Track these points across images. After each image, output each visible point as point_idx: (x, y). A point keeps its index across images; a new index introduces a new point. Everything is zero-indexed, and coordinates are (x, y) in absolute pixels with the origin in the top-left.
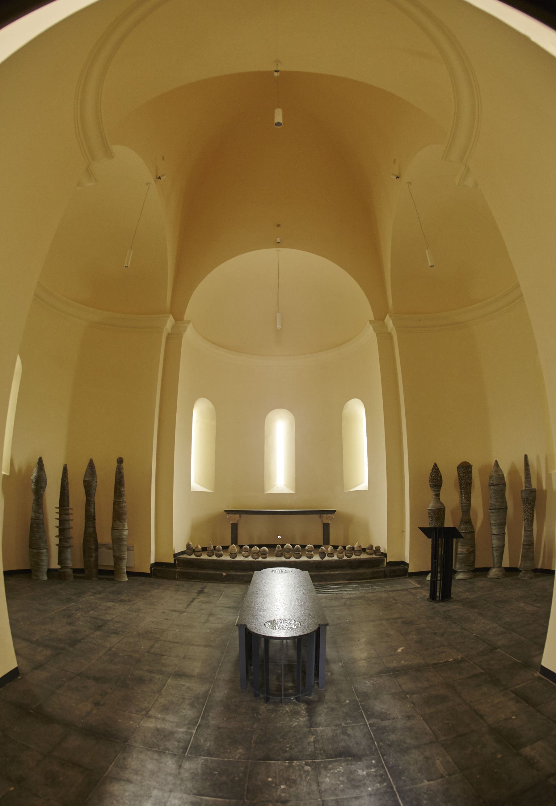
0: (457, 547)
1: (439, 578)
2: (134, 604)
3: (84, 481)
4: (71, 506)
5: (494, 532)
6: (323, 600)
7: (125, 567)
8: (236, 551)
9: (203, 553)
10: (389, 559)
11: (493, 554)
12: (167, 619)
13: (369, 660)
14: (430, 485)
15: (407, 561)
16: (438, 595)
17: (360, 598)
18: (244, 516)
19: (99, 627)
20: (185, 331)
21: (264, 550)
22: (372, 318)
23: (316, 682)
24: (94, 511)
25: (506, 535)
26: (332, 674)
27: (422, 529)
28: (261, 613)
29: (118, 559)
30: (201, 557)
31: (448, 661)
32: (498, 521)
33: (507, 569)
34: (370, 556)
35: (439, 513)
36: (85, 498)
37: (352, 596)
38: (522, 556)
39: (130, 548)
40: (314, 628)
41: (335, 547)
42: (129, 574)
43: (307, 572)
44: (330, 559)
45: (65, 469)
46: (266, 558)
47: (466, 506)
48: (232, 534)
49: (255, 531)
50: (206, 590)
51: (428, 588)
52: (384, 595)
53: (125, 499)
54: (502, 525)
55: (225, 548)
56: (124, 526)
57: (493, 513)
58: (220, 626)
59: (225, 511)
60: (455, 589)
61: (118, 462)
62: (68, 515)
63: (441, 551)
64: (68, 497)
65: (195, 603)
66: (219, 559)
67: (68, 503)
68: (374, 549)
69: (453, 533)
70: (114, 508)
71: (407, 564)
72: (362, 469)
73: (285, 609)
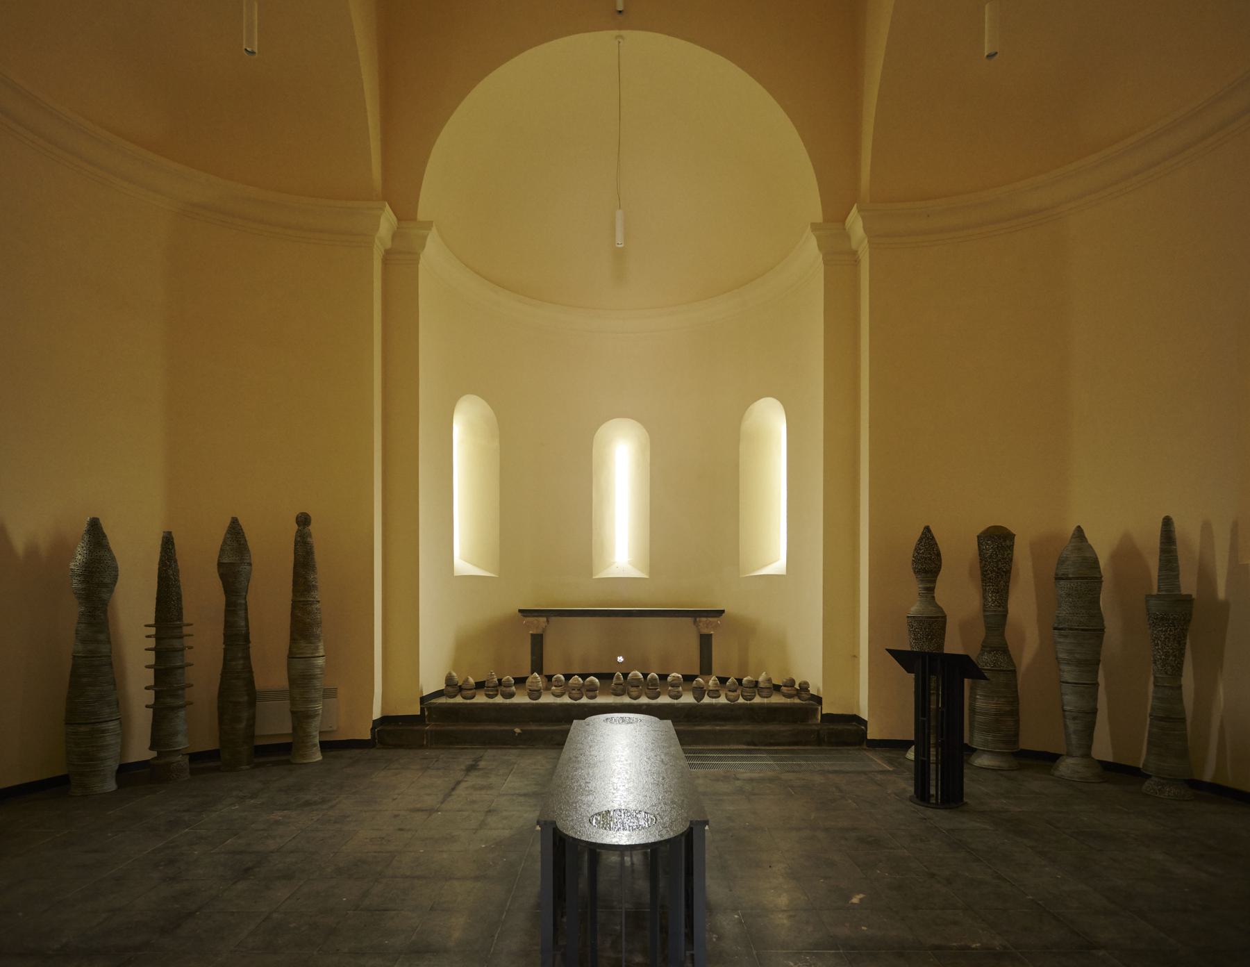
0: (973, 698)
1: (933, 758)
2: (332, 807)
3: (220, 565)
4: (187, 618)
5: (1068, 677)
6: (700, 781)
7: (316, 733)
8: (540, 685)
9: (478, 692)
10: (827, 709)
11: (1066, 726)
12: (401, 830)
13: (791, 913)
14: (914, 569)
15: (864, 715)
16: (933, 791)
17: (771, 780)
18: (553, 619)
19: (247, 870)
20: (423, 246)
21: (592, 683)
22: (818, 217)
23: (688, 953)
24: (247, 626)
25: (1101, 689)
26: (719, 939)
27: (895, 654)
28: (584, 798)
29: (301, 718)
30: (474, 701)
31: (969, 948)
32: (1077, 656)
33: (1106, 766)
34: (789, 701)
35: (933, 625)
36: (223, 598)
37: (755, 775)
38: (1149, 743)
39: (330, 693)
40: (681, 828)
41: (723, 680)
42: (326, 746)
43: (669, 722)
44: (714, 701)
45: (168, 543)
46: (594, 697)
47: (996, 617)
48: (533, 653)
49: (576, 646)
50: (482, 764)
51: (910, 775)
52: (818, 779)
53: (317, 595)
54: (1090, 664)
55: (520, 681)
56: (316, 649)
57: (1066, 636)
58: (507, 833)
59: (520, 611)
60: (971, 787)
61: (297, 522)
62: (181, 637)
63: (935, 703)
64: (179, 599)
65: (461, 790)
66: (508, 701)
67: (180, 610)
68: (797, 686)
69: (962, 667)
70: (293, 614)
71: (864, 722)
72: (774, 536)
73: (628, 790)
